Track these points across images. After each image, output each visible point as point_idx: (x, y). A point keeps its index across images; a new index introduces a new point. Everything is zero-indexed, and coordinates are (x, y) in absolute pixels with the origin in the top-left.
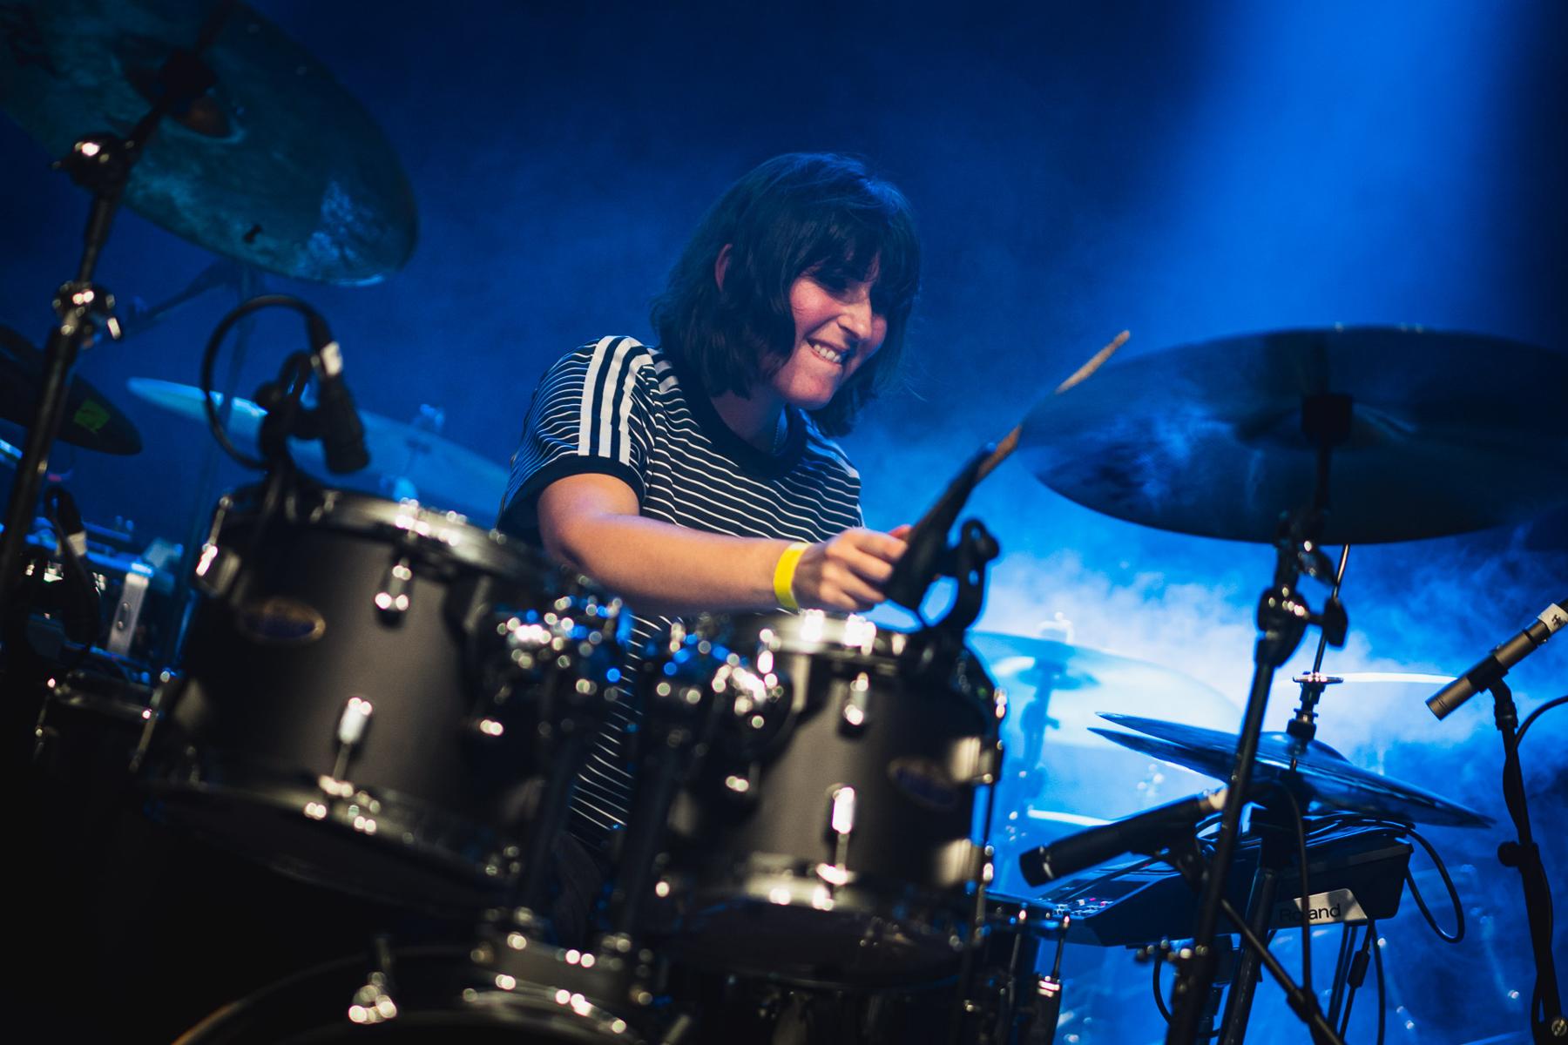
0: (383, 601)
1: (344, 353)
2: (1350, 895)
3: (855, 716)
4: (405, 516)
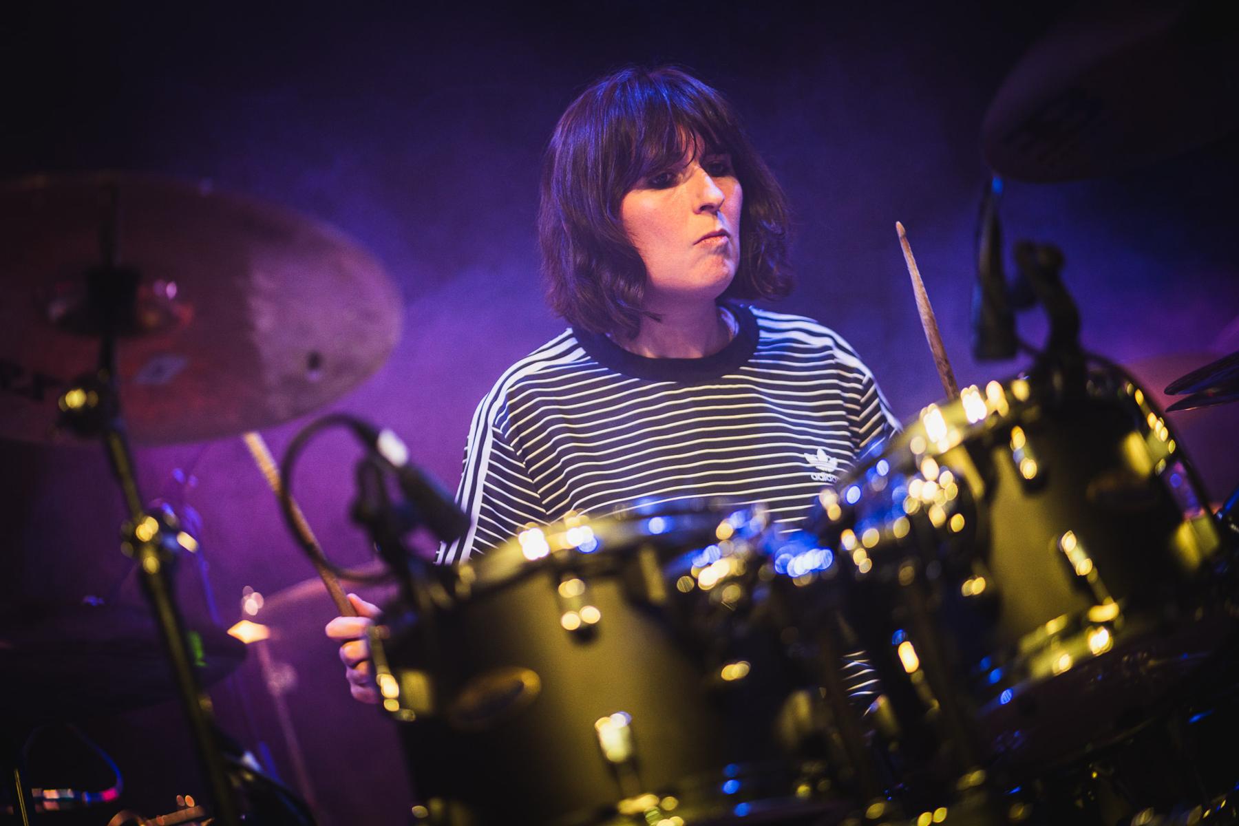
0: (571, 621)
1: (402, 436)
3: (1029, 469)
4: (532, 543)
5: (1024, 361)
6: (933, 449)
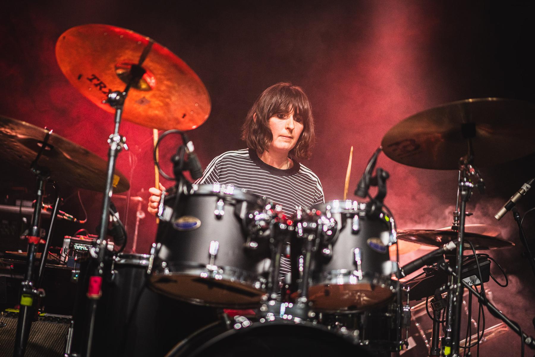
0: (217, 212)
2: (476, 277)
4: (216, 187)
5: (367, 200)
6: (333, 211)
